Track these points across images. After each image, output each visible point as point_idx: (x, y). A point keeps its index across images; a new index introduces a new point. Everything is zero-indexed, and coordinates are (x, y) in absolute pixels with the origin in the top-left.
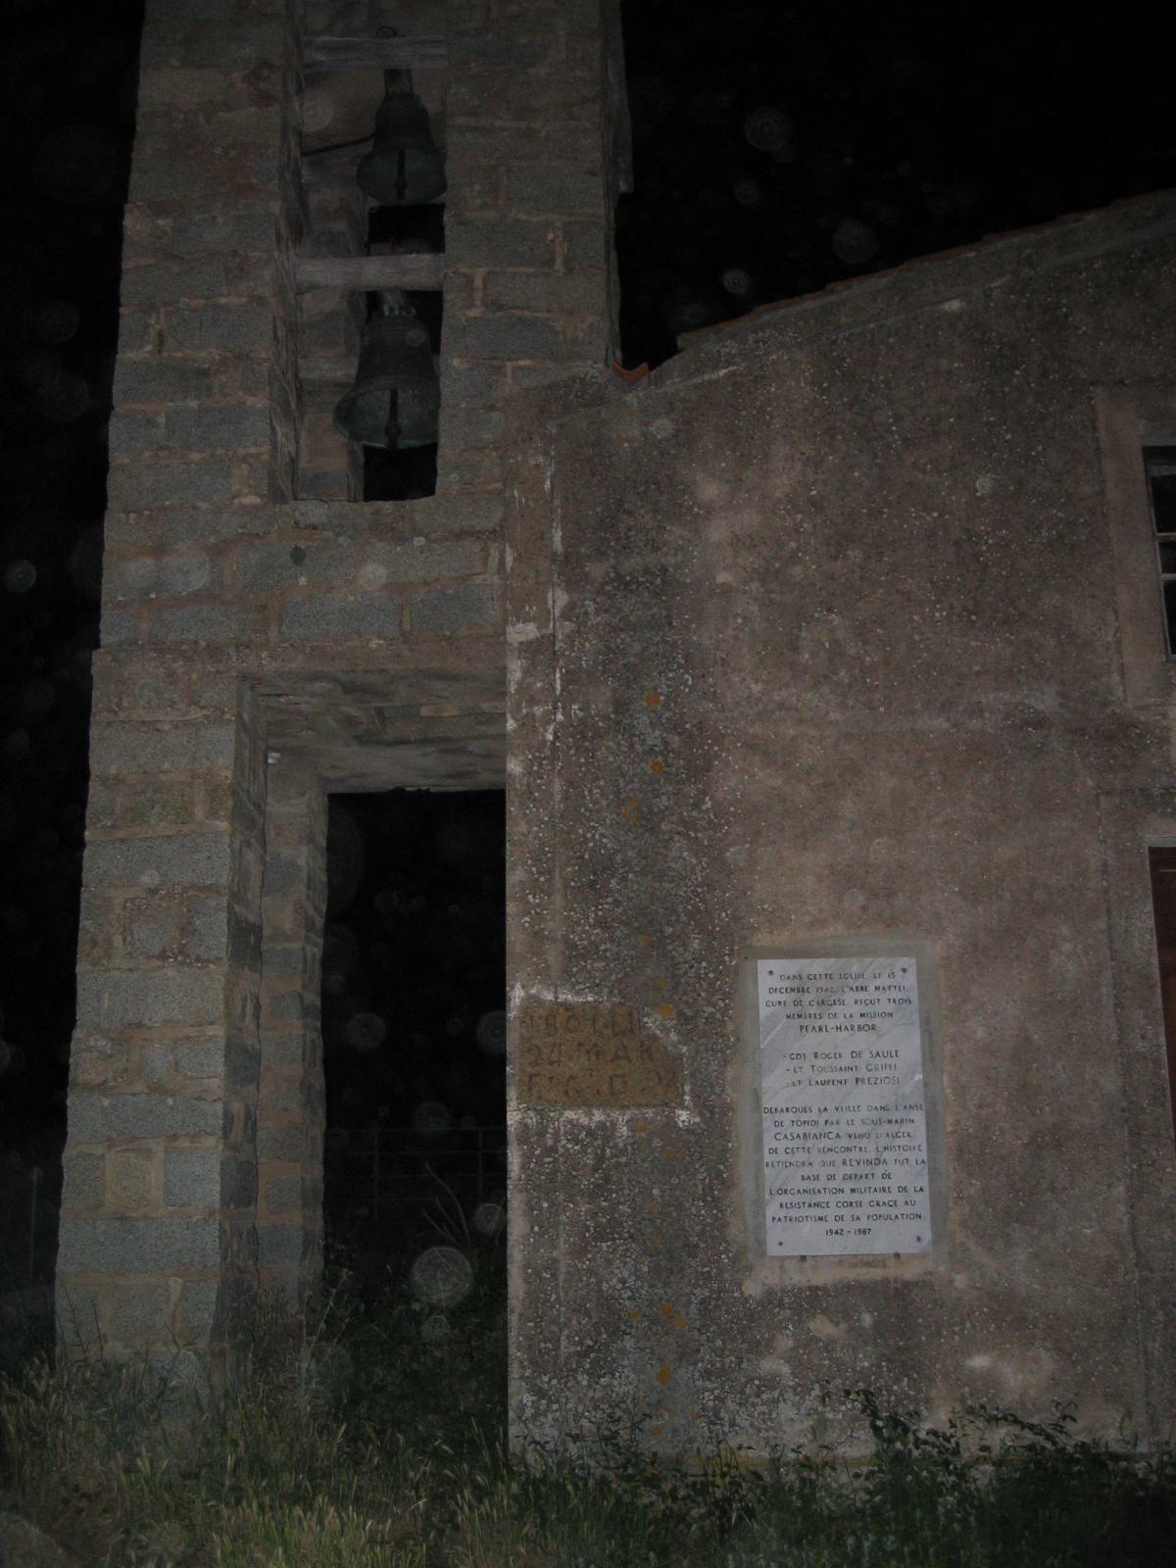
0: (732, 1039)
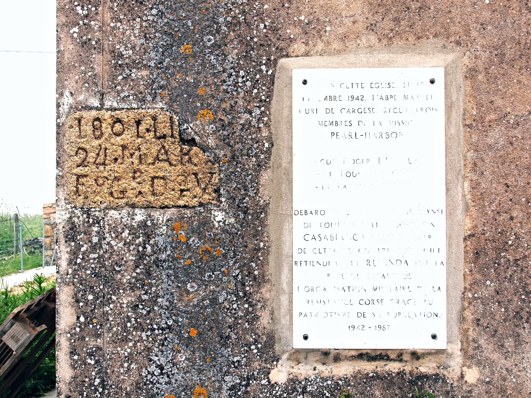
0: (267, 145)
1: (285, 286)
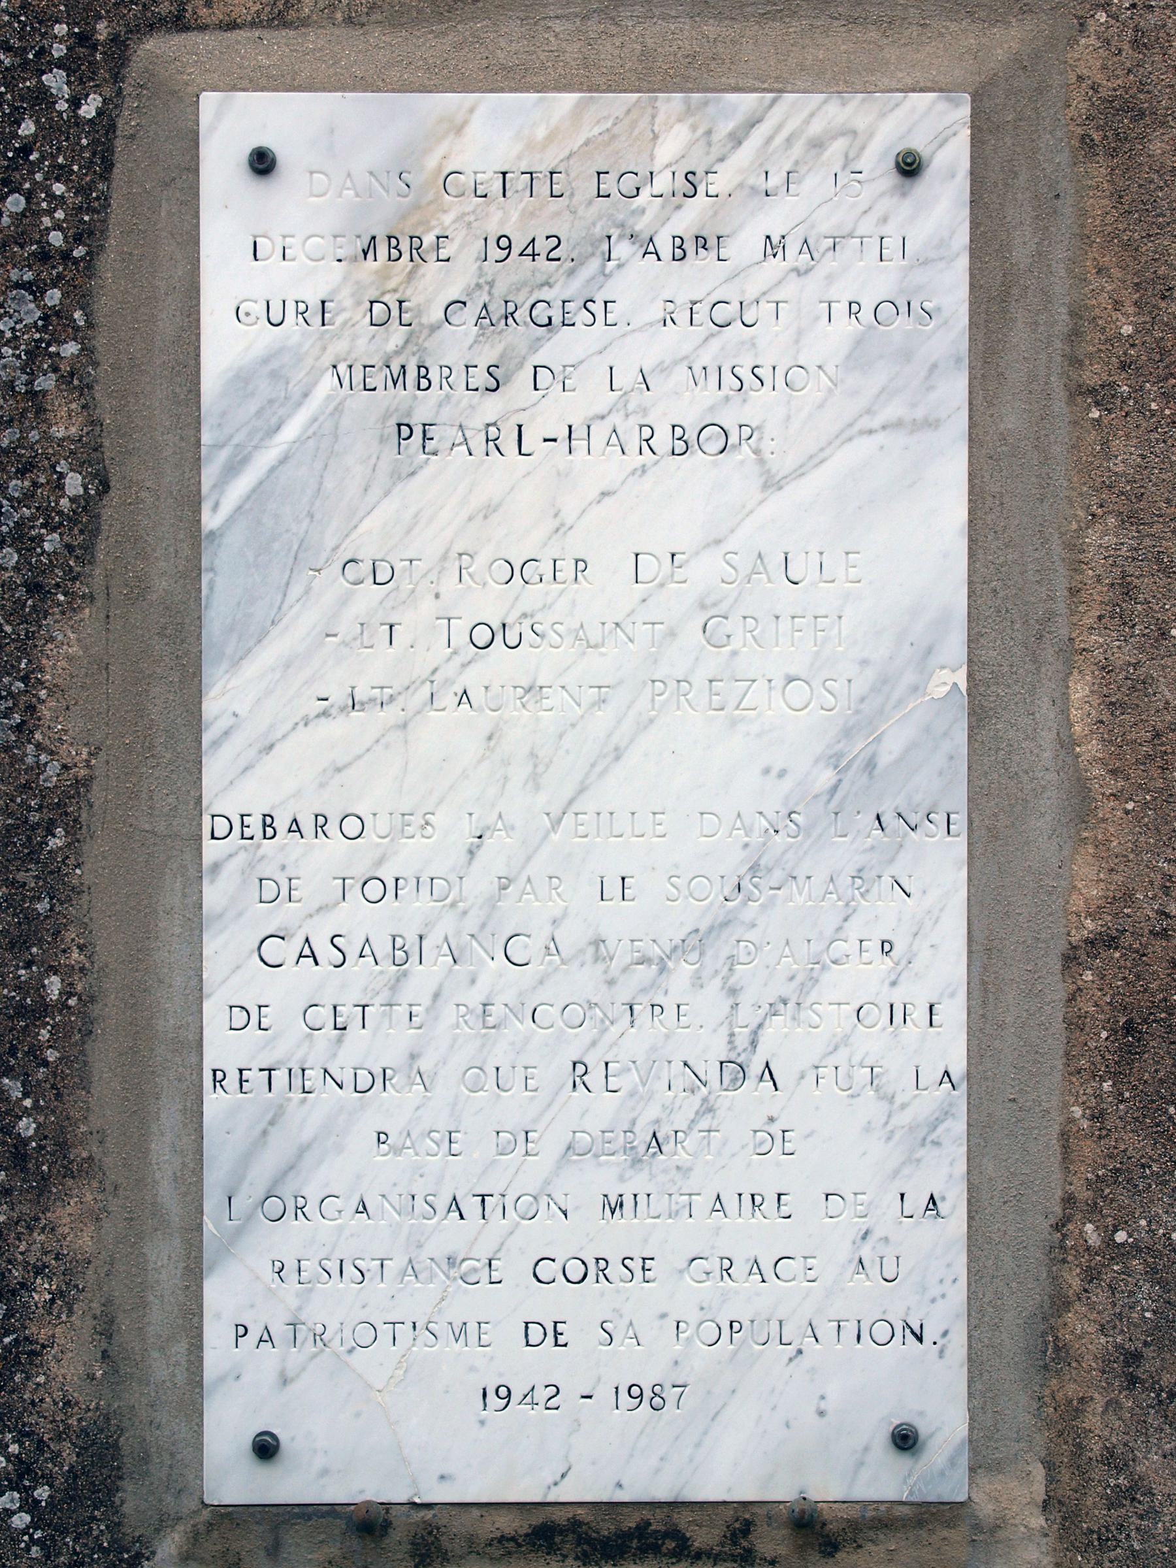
0: (74, 484)
1: (166, 1193)
